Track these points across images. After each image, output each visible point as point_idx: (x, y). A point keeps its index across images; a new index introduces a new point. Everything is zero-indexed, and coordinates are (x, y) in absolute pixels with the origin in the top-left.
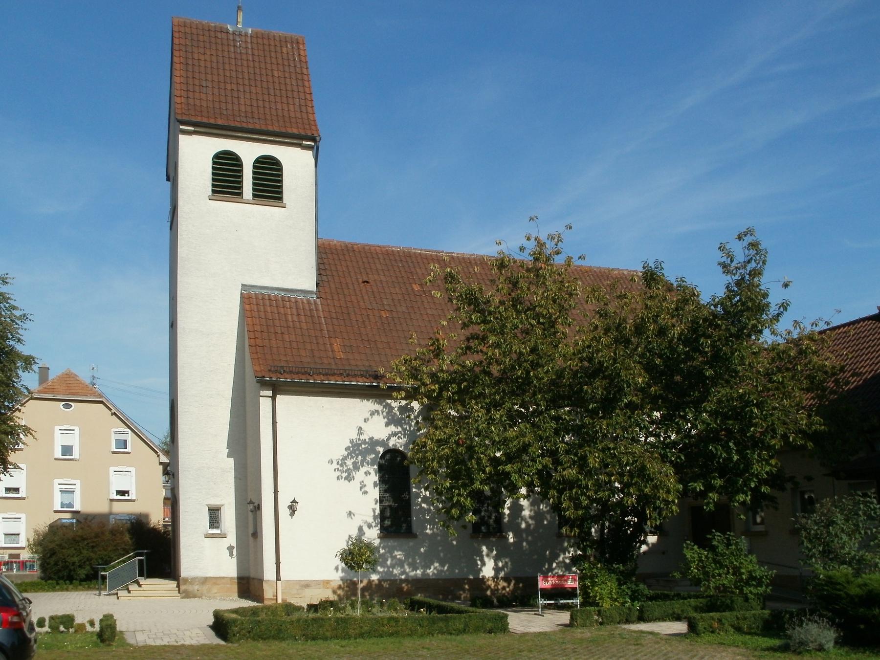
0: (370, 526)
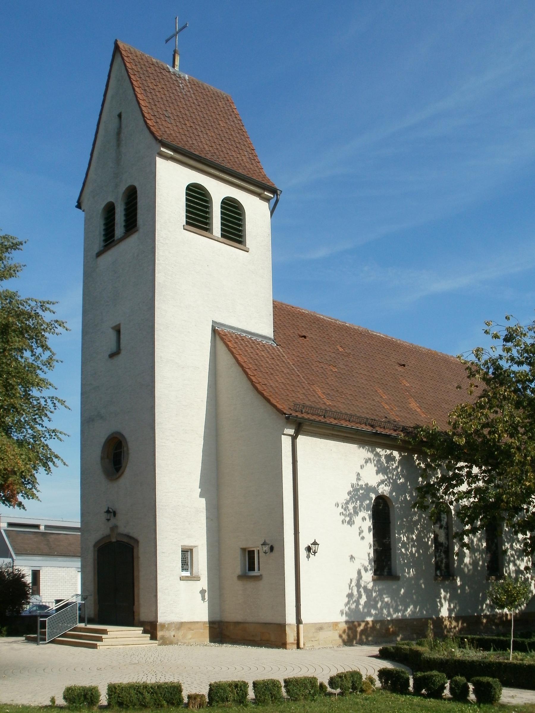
0: (366, 570)
